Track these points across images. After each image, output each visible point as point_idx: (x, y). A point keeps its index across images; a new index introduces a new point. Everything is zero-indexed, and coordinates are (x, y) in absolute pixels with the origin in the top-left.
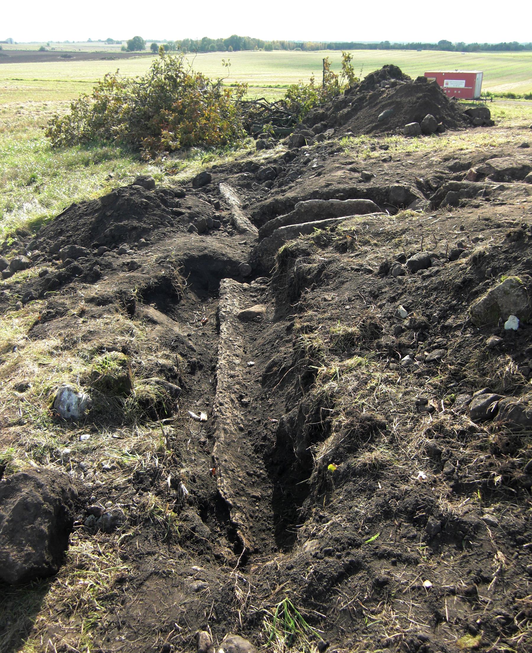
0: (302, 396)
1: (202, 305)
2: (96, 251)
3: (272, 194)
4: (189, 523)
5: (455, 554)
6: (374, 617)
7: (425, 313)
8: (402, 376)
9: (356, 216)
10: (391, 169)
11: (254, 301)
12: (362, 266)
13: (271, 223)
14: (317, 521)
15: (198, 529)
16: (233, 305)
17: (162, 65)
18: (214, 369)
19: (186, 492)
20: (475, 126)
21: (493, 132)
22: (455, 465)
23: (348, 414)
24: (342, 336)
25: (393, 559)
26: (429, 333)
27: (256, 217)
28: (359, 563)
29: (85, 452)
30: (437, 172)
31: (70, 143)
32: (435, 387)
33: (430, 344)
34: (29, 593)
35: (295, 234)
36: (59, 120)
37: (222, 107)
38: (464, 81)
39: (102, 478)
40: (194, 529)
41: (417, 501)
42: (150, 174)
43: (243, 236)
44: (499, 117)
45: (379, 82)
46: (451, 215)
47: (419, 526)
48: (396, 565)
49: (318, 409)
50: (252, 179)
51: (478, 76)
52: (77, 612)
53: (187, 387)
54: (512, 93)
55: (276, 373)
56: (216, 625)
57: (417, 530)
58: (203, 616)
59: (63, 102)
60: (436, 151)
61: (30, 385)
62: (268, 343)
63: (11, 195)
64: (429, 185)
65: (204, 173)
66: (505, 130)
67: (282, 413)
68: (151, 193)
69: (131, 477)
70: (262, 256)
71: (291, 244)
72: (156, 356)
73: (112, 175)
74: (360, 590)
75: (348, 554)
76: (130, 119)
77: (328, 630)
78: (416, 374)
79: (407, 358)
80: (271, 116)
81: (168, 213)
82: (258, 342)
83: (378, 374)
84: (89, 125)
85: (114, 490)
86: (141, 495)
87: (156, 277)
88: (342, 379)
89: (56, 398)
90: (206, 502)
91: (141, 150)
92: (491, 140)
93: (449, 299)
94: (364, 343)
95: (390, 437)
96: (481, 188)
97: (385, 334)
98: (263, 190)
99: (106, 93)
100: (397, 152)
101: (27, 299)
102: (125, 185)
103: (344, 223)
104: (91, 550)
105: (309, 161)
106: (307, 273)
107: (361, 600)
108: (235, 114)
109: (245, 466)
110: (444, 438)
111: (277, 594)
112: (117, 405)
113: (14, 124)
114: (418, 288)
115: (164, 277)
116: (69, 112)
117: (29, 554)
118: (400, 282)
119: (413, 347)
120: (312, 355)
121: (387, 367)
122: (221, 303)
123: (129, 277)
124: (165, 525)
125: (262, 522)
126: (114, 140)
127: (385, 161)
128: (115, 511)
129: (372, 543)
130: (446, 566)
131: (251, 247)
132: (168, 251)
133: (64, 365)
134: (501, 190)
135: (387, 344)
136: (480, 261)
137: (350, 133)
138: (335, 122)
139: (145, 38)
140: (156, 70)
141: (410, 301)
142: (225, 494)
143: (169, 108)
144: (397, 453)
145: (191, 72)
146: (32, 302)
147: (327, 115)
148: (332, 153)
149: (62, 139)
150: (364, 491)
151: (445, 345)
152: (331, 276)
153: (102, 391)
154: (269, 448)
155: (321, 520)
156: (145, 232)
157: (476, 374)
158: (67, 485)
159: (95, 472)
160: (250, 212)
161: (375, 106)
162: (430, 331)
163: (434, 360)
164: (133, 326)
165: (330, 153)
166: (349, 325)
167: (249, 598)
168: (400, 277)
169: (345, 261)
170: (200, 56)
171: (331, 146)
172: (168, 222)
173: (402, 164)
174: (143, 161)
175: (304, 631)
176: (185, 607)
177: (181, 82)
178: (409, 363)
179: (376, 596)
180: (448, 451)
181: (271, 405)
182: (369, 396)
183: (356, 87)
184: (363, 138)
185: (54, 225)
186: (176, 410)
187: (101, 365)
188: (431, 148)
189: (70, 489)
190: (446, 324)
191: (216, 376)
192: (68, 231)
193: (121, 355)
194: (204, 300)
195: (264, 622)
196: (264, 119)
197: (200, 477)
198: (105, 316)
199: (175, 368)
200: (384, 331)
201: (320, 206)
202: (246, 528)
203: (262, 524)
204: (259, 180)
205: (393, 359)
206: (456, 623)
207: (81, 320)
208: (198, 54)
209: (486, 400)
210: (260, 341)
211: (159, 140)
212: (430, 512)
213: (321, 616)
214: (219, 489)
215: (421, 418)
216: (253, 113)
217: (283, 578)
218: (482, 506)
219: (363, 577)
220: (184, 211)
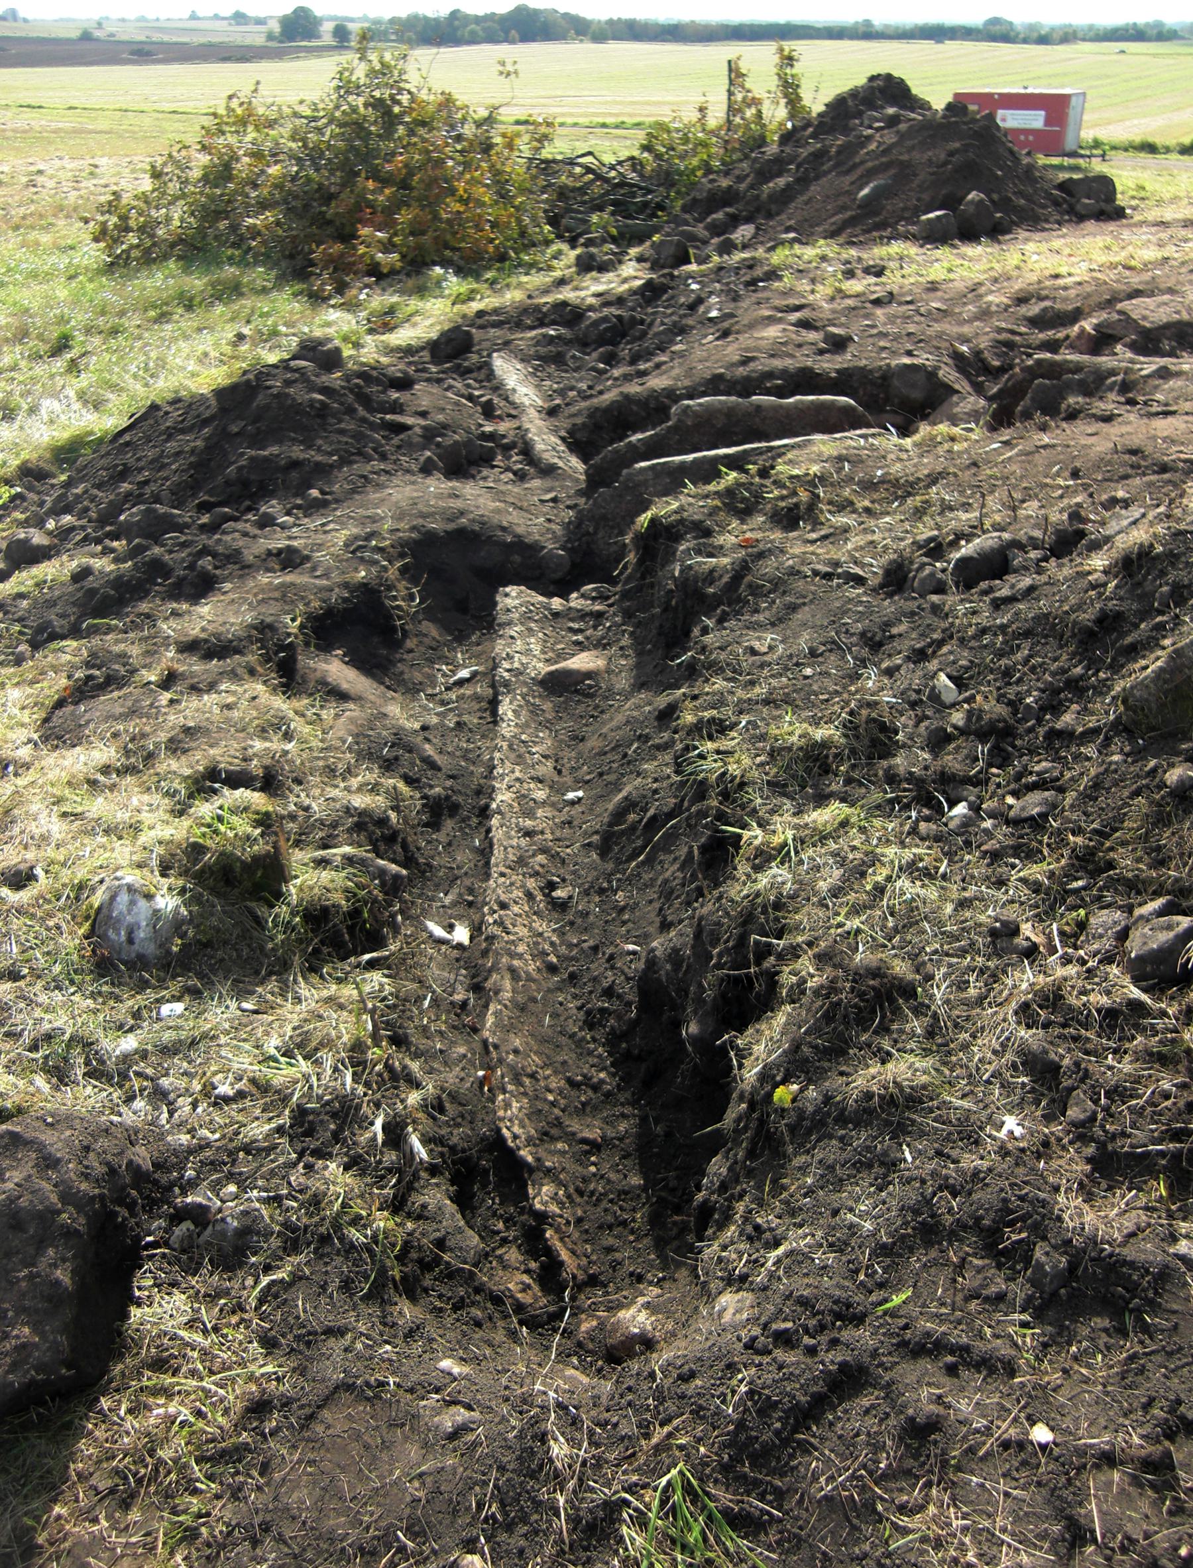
0: (702, 895)
1: (454, 650)
2: (205, 519)
3: (616, 379)
4: (429, 1227)
5: (1108, 1348)
6: (904, 1521)
7: (1004, 695)
8: (950, 855)
9: (817, 437)
10: (893, 323)
11: (577, 643)
12: (837, 564)
13: (616, 451)
14: (750, 1239)
15: (450, 1243)
16: (528, 652)
17: (360, 73)
18: (484, 813)
19: (421, 1152)
20: (1081, 218)
21: (1126, 234)
22: (1096, 1102)
23: (822, 959)
24: (801, 749)
25: (950, 1359)
26: (1014, 747)
27: (578, 436)
28: (862, 1370)
29: (169, 1051)
30: (1000, 330)
31: (150, 257)
32: (1036, 888)
33: (1018, 777)
34: (26, 1439)
35: (672, 481)
36: (124, 201)
37: (496, 173)
38: (1043, 113)
39: (211, 1122)
40: (441, 1244)
41: (1005, 1201)
42: (331, 331)
43: (548, 483)
44: (1133, 198)
45: (859, 114)
46: (1046, 439)
47: (1012, 1268)
48: (957, 1376)
49: (742, 940)
50: (568, 343)
51: (1073, 101)
52: (147, 1493)
53: (422, 860)
54: (1151, 140)
55: (633, 828)
56: (502, 1537)
57: (1008, 1279)
58: (469, 1508)
59: (136, 159)
60: (996, 280)
61: (38, 871)
62: (613, 749)
63: (13, 379)
64: (983, 361)
65: (456, 329)
66: (1153, 229)
67: (651, 929)
68: (335, 378)
69: (285, 1119)
70: (595, 533)
71: (664, 508)
72: (347, 789)
73: (246, 331)
74: (868, 1444)
75: (834, 1342)
76: (286, 202)
77: (788, 1552)
78: (986, 852)
79: (961, 809)
80: (607, 193)
81: (372, 426)
82: (590, 744)
83: (891, 852)
84: (192, 214)
85: (241, 1155)
86: (309, 1167)
87: (346, 585)
88: (801, 862)
89: (99, 909)
90: (468, 1159)
91: (312, 274)
92: (1124, 254)
93: (1063, 661)
94: (853, 767)
95: (927, 1020)
96: (1113, 372)
97: (904, 746)
98: (594, 369)
99: (232, 139)
100: (906, 282)
101: (42, 638)
102: (272, 358)
103: (789, 456)
104: (185, 1319)
105: (700, 301)
106: (704, 580)
107: (871, 1473)
108: (523, 191)
109: (564, 1063)
110: (1064, 1026)
111: (658, 1449)
112: (249, 923)
113: (22, 211)
114: (984, 631)
115: (364, 587)
116: (147, 184)
117: (24, 1346)
118: (936, 609)
119: (979, 781)
120: (726, 796)
121: (914, 831)
122: (500, 647)
123: (282, 585)
124: (370, 1251)
125: (605, 1204)
126: (250, 249)
127: (877, 302)
128: (245, 1213)
129: (893, 1313)
130: (1086, 1381)
131: (568, 507)
132: (374, 519)
133: (123, 816)
134: (1162, 377)
135: (911, 773)
136: (1140, 567)
137: (792, 235)
138: (758, 210)
139: (318, 12)
140: (346, 87)
141: (963, 662)
142: (515, 1137)
143: (375, 175)
144: (945, 1064)
145: (425, 91)
146: (55, 645)
147: (737, 193)
148: (753, 283)
149: (132, 247)
150: (870, 1166)
151: (1058, 779)
152: (765, 591)
153: (213, 891)
154: (619, 1018)
155: (757, 1235)
156: (322, 471)
157: (1139, 860)
158: (122, 1153)
159: (195, 1105)
160: (564, 424)
161: (848, 172)
162: (1018, 743)
163: (1032, 818)
164: (291, 714)
165: (748, 284)
166: (816, 722)
167: (584, 1463)
168: (935, 598)
169: (797, 550)
170: (447, 53)
171: (751, 267)
172: (374, 450)
173: (917, 311)
174: (317, 299)
175: (727, 1553)
176: (423, 1484)
177: (403, 113)
178: (967, 823)
179: (909, 1463)
180: (1077, 1064)
181: (622, 910)
182: (871, 907)
183: (805, 128)
184: (823, 247)
185: (108, 454)
186: (396, 929)
187: (209, 826)
188: (985, 272)
189: (130, 1163)
190: (1059, 726)
191: (489, 831)
192: (140, 470)
193: (256, 799)
194: (460, 637)
195: (625, 1528)
196: (593, 200)
197: (454, 1097)
198: (223, 687)
199: (393, 815)
200: (900, 737)
201: (730, 412)
202: (568, 1223)
203: (606, 1210)
204: (584, 344)
205: (926, 812)
206: (1124, 1550)
207: (165, 697)
208: (442, 50)
209: (1171, 934)
210: (593, 743)
211: (354, 248)
212: (1039, 1232)
213: (769, 1513)
214: (502, 1125)
215: (1005, 972)
216: (566, 186)
217: (670, 1406)
218: (1171, 1216)
219: (873, 1407)
220: (410, 421)
